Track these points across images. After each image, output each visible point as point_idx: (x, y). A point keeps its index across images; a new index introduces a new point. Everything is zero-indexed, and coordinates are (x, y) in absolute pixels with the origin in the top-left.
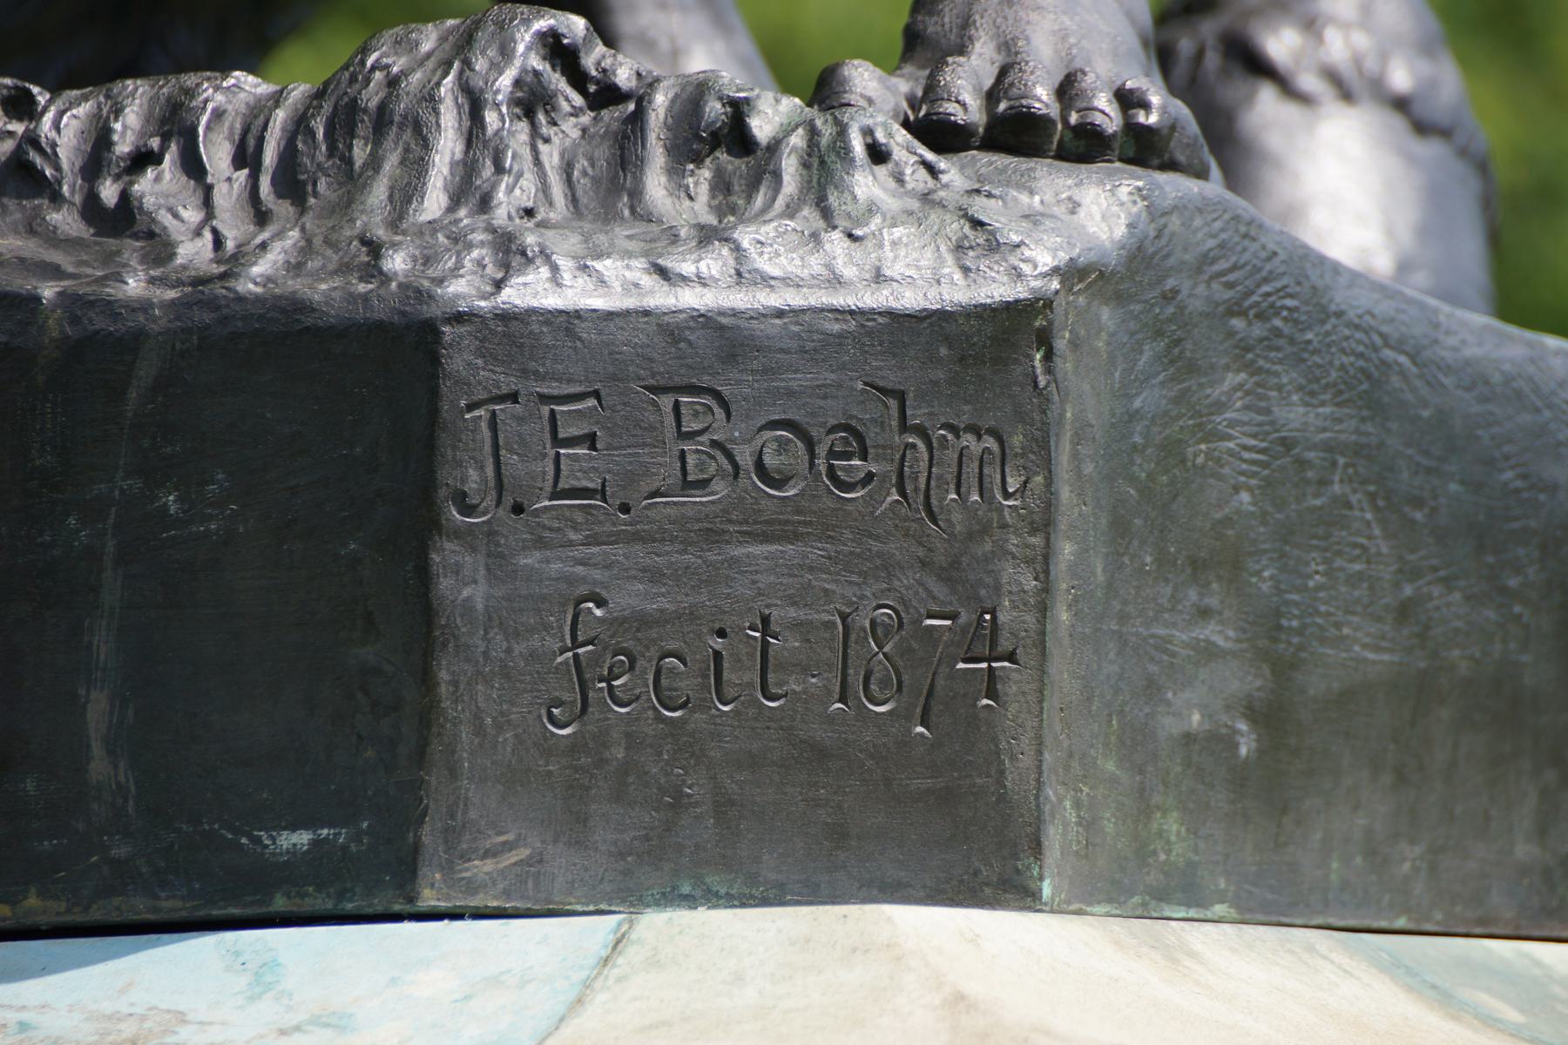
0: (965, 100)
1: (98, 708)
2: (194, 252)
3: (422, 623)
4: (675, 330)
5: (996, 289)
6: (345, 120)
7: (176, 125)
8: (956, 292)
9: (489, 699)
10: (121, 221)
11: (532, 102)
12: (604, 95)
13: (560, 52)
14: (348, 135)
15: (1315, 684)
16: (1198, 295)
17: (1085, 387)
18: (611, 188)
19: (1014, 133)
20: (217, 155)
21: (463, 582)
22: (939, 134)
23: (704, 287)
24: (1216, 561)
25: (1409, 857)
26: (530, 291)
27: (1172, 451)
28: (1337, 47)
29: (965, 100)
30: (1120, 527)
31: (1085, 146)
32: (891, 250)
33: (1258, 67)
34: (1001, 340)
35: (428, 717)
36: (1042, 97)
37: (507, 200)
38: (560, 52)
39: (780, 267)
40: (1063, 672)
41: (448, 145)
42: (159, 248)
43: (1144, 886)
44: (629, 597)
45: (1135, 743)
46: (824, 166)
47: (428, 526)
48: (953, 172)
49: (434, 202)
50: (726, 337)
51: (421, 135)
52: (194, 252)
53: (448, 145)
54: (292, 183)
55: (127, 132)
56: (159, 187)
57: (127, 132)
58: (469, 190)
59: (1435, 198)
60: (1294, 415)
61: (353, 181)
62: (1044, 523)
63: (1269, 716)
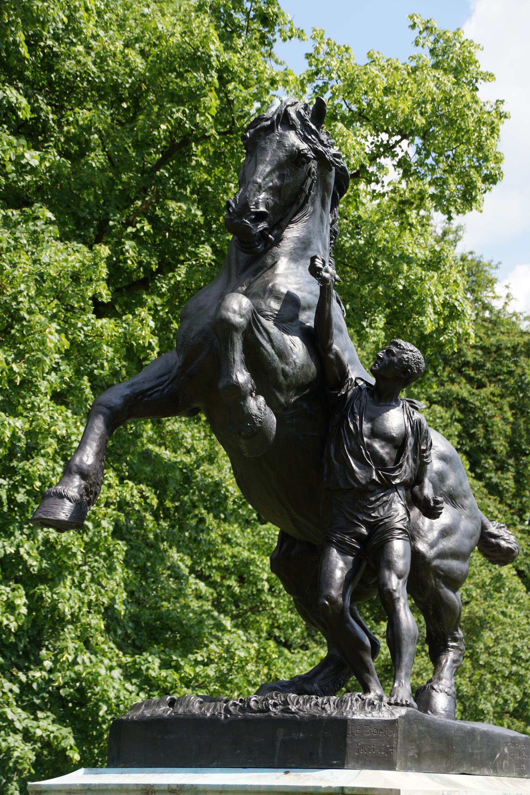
0: (393, 701)
1: (320, 750)
2: (329, 712)
3: (345, 745)
4: (366, 721)
5: (393, 718)
6: (342, 701)
7: (328, 701)
8: (390, 718)
9: (351, 752)
10: (323, 709)
11: (357, 700)
12: (363, 700)
13: (359, 696)
14: (342, 703)
15: (423, 751)
16: (412, 718)
17: (401, 727)
18: (362, 708)
19: (396, 704)
20: (332, 703)
21: (349, 741)
22: (390, 704)
23: (369, 717)
24: (413, 741)
25: (432, 766)
26: (355, 717)
27: (409, 732)
28: (441, 687)
29: (393, 701)
30: (404, 738)
31: (402, 705)
32: (384, 714)
33: (434, 689)
34: (393, 723)
35: (346, 752)
36: (399, 701)
37: (354, 708)
38: (359, 696)
39: (375, 716)
40: (399, 750)
41: (349, 704)
42: (326, 711)
43: (406, 768)
44: (362, 743)
45: (406, 757)
46: (380, 707)
47: (346, 736)
48: (391, 707)
49: (348, 709)
50: (371, 722)
51: (347, 703)
52: (329, 712)
53: (349, 704)
54: (337, 706)
55: (325, 701)
56: (327, 706)
57: (325, 701)
58: (351, 708)
59: (449, 701)
60: (421, 728)
61: (342, 706)
62: (397, 738)
63: (419, 754)
